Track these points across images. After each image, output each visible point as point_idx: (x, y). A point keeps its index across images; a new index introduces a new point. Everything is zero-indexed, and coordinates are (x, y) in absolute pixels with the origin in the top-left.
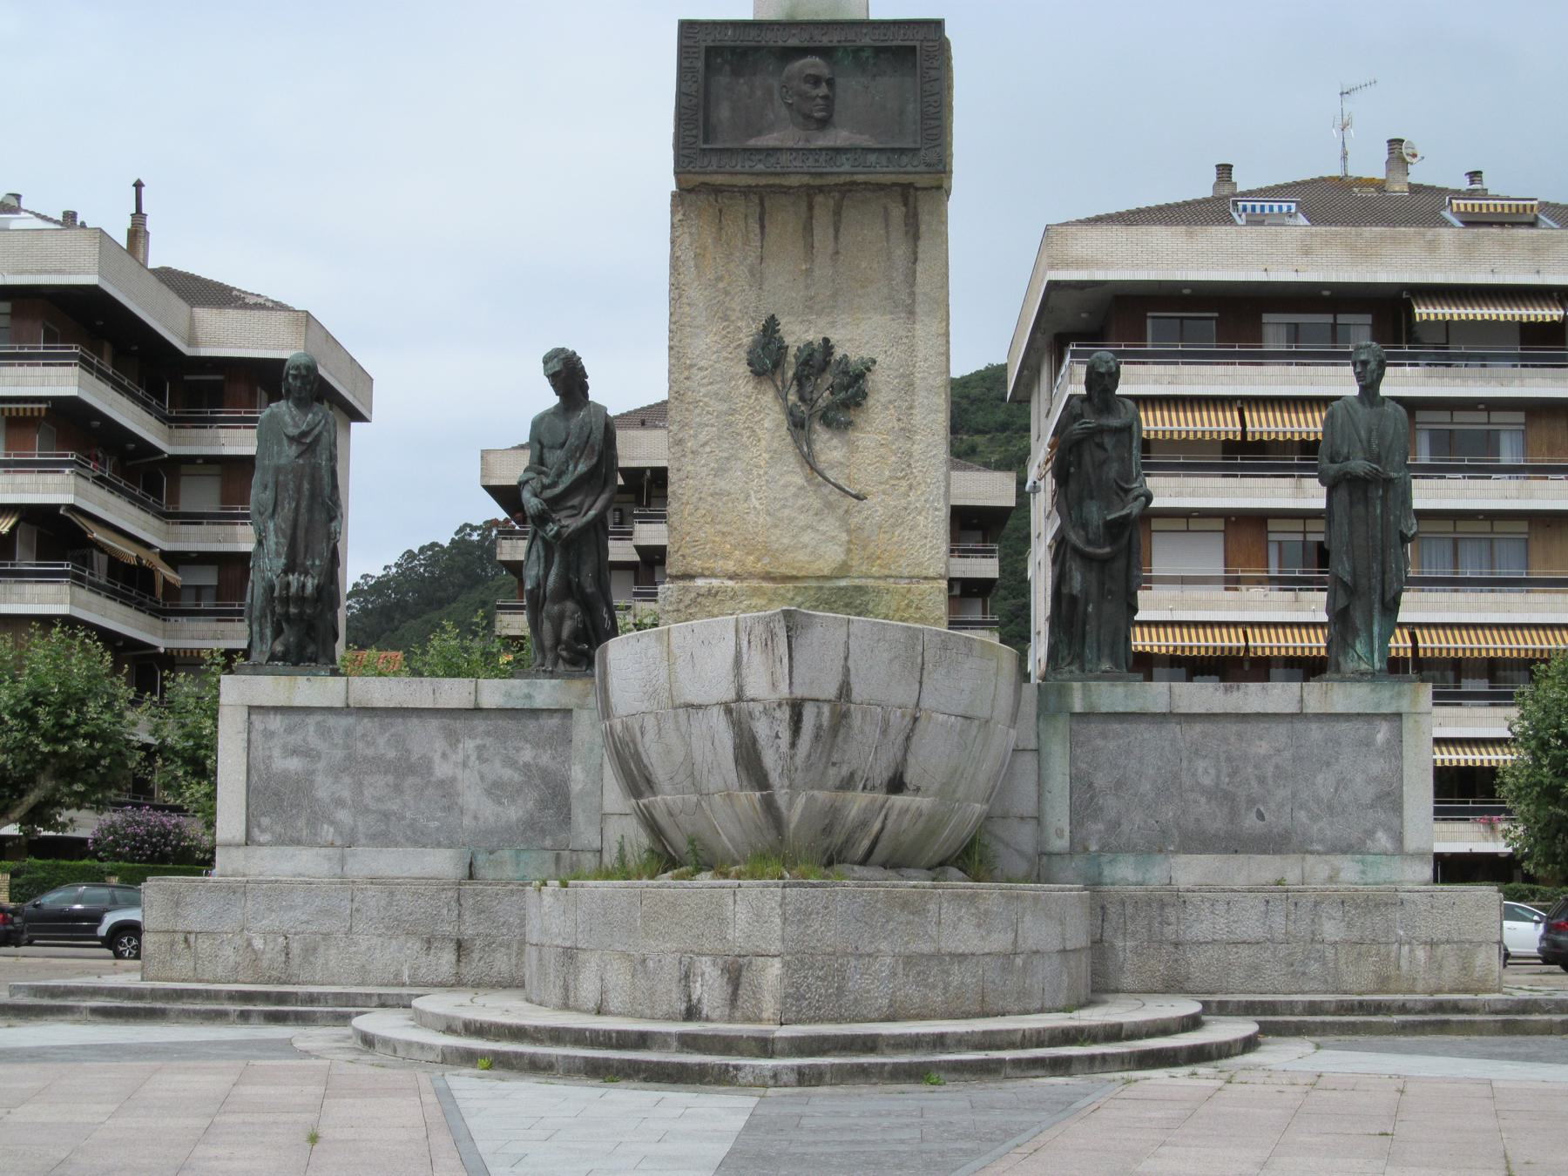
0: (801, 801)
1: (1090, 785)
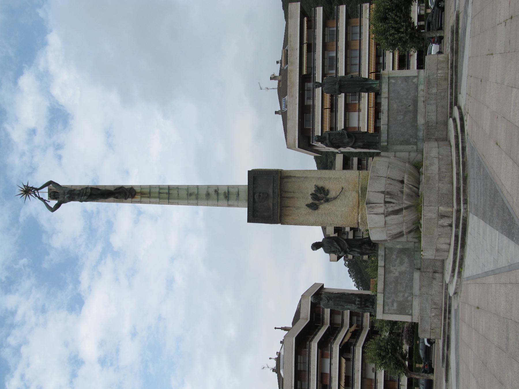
0: (406, 202)
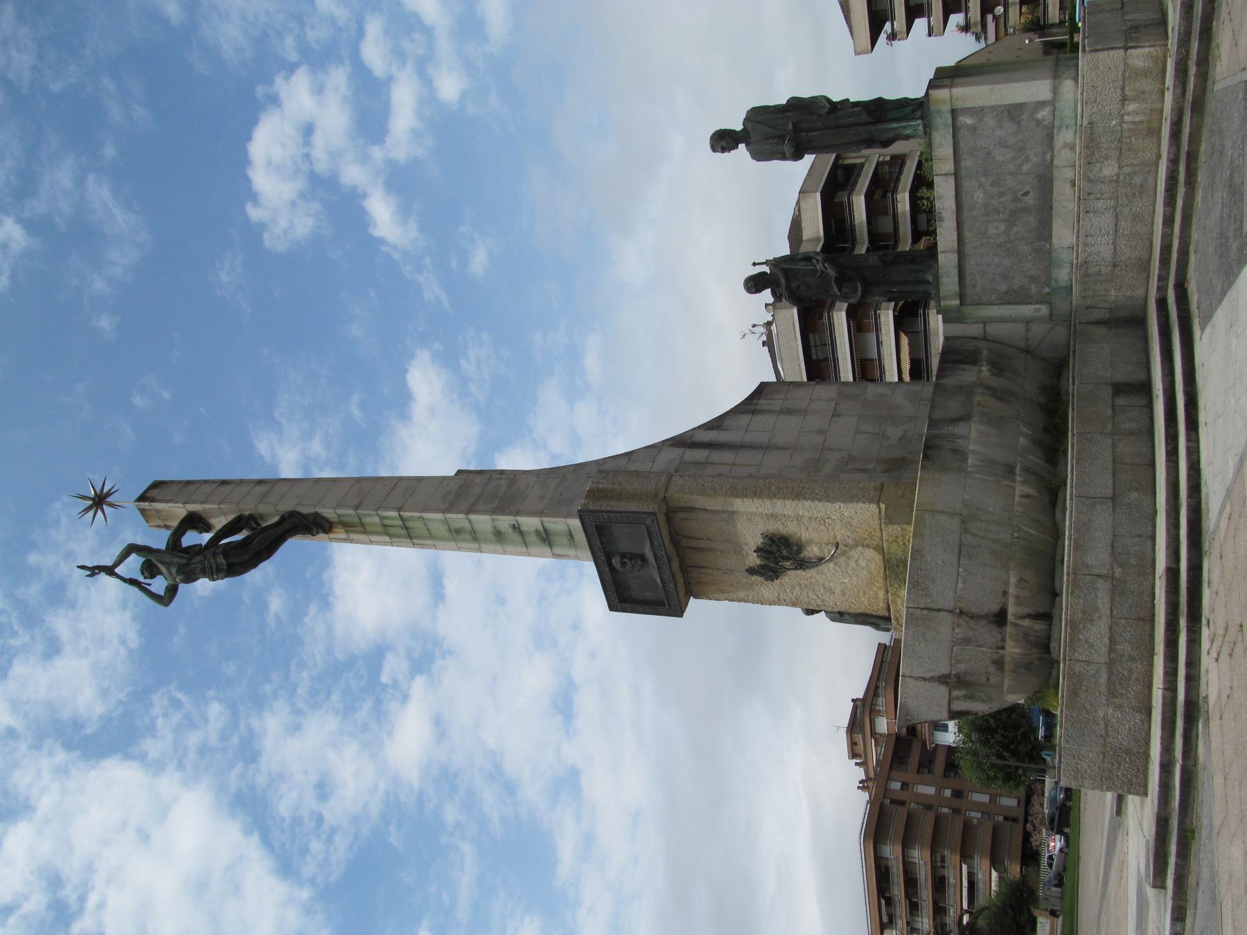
1: (1006, 293)
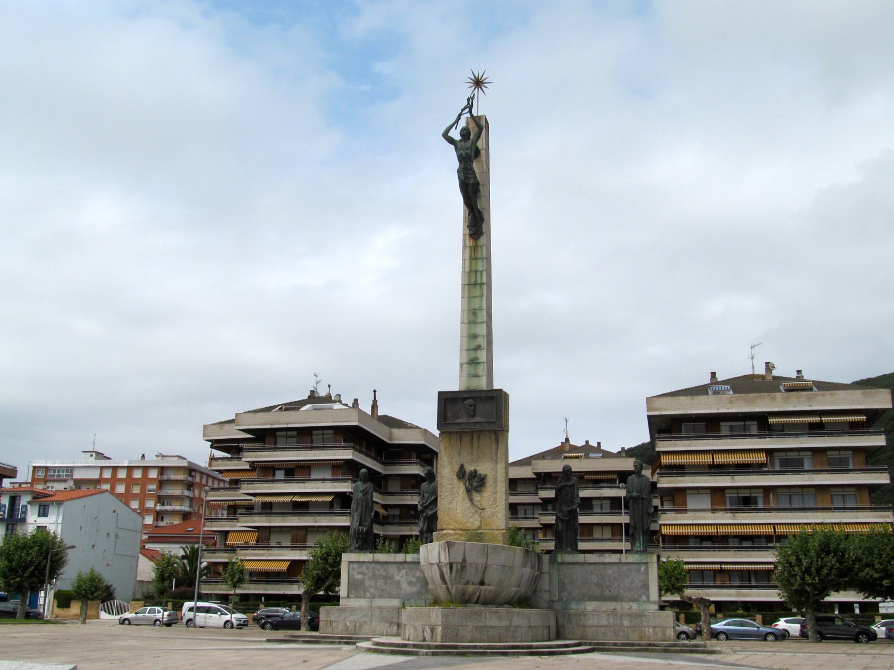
0: (454, 588)
